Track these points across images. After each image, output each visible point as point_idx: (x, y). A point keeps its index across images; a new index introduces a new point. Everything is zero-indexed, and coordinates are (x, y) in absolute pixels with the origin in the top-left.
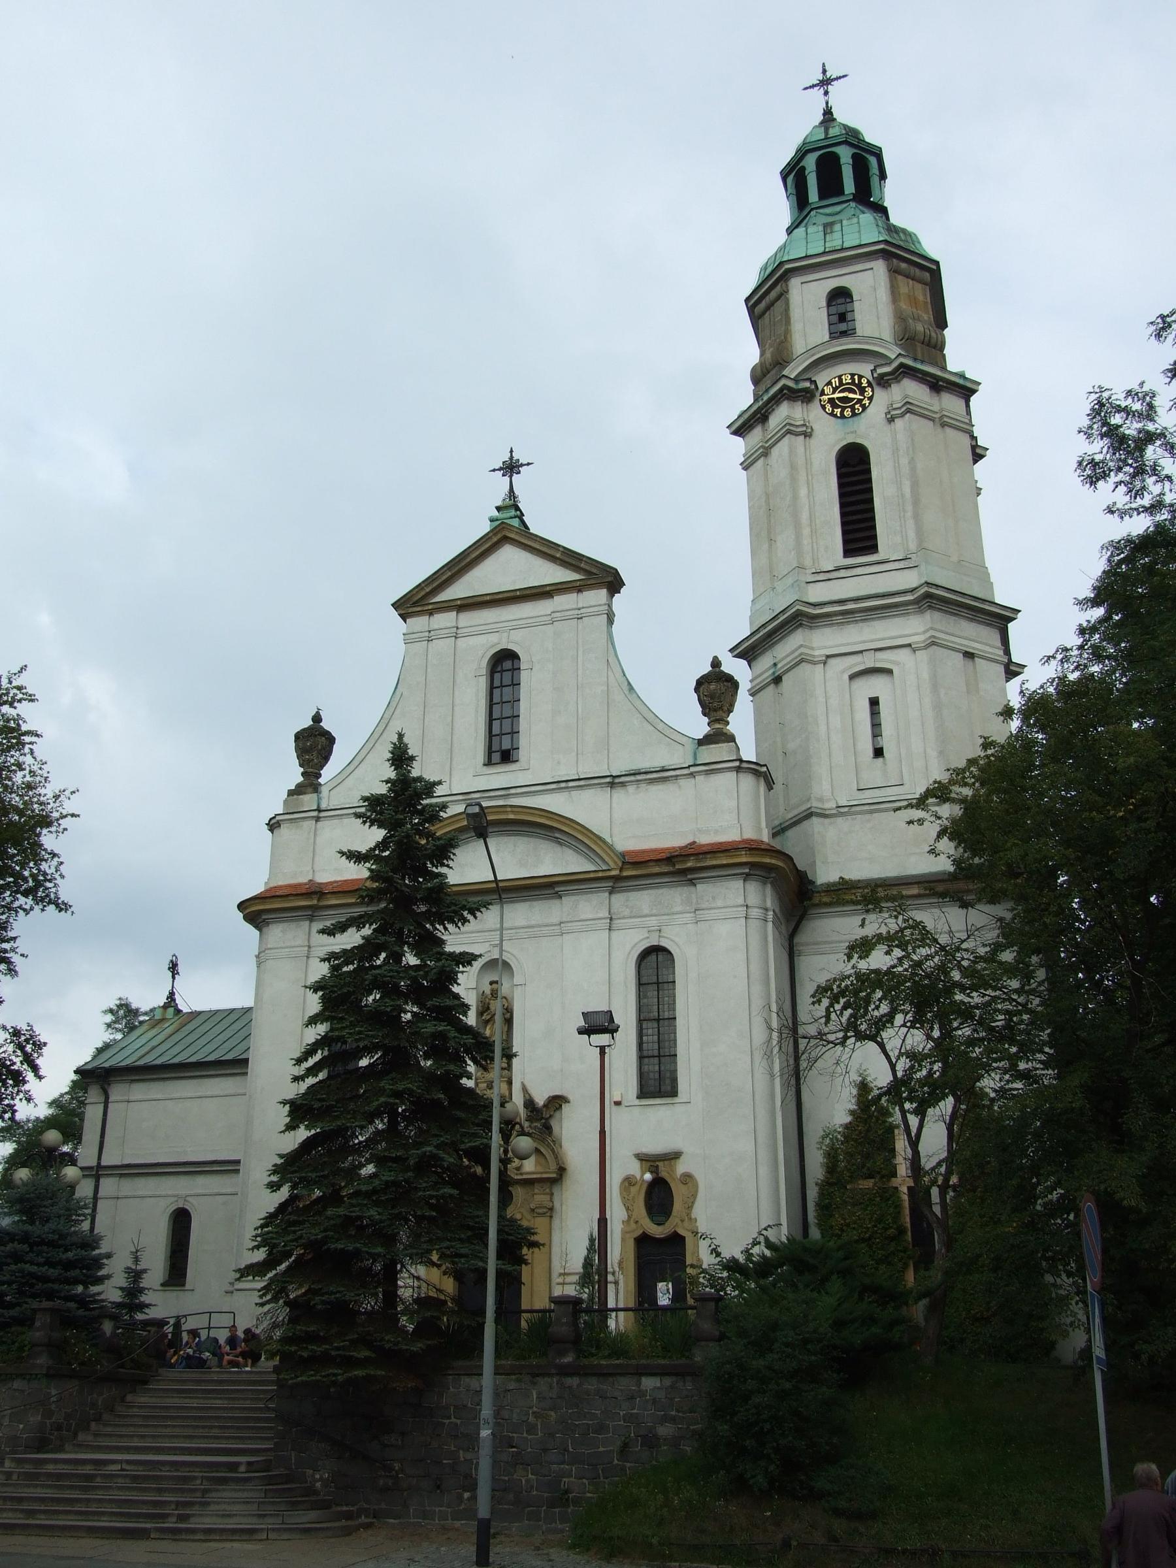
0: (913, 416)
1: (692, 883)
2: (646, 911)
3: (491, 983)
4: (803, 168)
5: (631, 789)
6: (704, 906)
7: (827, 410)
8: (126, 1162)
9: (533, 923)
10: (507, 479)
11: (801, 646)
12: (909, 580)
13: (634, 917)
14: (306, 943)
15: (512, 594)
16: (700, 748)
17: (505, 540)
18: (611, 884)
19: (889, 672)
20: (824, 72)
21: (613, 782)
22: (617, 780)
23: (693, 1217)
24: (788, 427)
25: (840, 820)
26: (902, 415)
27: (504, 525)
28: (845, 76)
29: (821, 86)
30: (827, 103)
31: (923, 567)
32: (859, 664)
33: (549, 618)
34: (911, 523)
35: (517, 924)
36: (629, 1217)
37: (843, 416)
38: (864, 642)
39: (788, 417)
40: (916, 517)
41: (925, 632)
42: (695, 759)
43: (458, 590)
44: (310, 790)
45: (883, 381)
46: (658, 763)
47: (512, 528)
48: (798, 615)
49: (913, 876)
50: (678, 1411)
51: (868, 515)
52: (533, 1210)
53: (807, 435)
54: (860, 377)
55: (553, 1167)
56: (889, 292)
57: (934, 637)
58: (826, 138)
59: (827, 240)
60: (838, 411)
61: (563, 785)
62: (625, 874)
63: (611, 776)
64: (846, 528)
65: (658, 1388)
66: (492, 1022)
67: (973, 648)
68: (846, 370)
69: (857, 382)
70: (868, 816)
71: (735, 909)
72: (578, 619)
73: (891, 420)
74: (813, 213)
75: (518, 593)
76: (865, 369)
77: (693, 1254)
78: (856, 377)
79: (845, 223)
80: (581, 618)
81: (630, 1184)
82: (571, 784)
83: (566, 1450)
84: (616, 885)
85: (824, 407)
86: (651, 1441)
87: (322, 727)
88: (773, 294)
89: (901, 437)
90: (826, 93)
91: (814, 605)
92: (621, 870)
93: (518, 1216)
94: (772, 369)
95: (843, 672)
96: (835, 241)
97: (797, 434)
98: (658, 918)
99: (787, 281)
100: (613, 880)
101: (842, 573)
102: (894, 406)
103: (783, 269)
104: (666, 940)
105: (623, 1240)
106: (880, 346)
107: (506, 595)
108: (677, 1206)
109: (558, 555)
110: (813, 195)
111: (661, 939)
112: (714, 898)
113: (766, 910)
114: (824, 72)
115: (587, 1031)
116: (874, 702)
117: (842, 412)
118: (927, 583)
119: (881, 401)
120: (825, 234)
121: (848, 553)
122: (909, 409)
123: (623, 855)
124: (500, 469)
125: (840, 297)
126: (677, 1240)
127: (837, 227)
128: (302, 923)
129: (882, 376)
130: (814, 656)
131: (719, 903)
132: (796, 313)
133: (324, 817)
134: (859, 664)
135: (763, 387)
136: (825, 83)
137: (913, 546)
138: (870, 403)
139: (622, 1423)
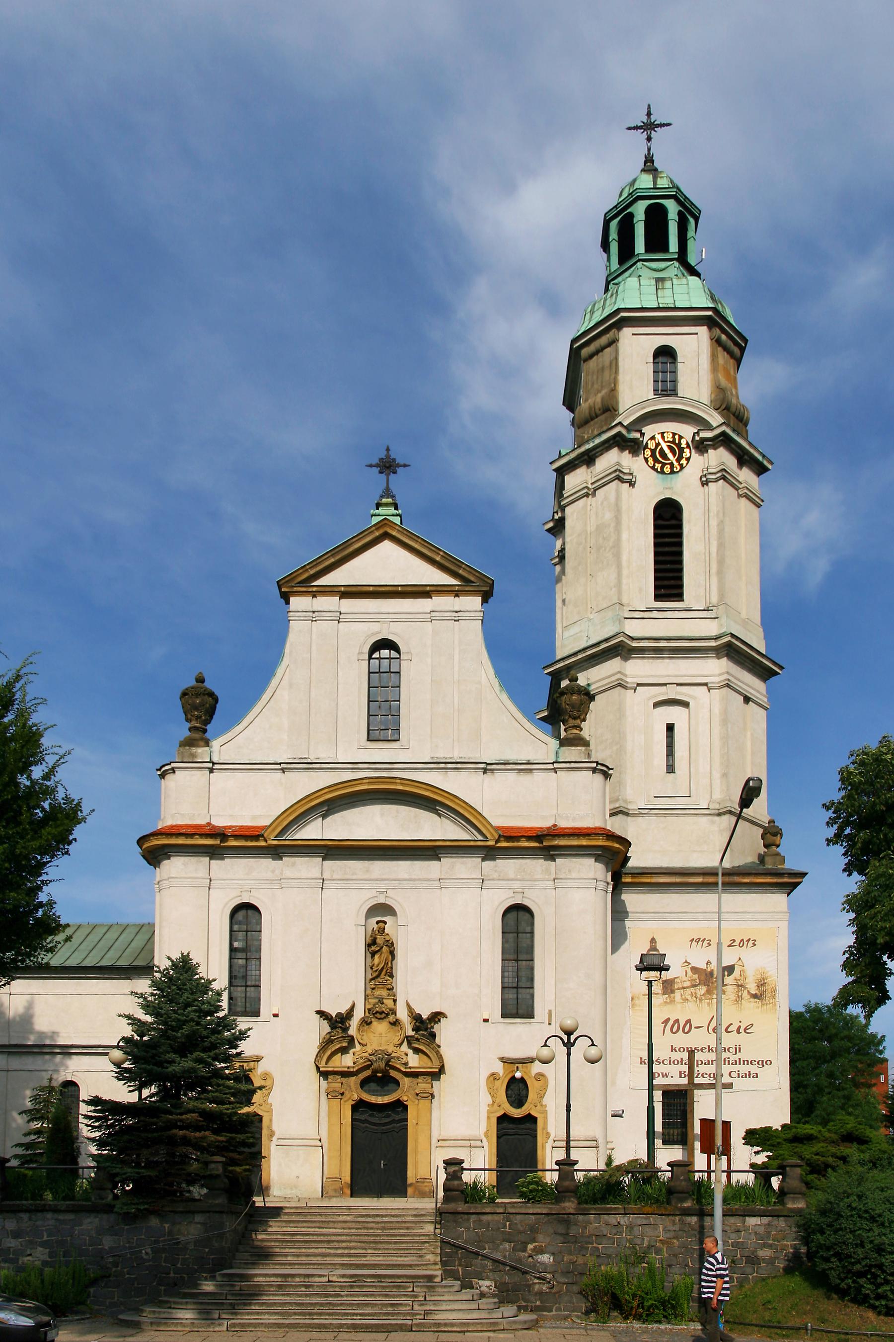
0: (725, 483)
1: (552, 858)
2: (512, 876)
3: (378, 922)
4: (631, 216)
5: (498, 775)
6: (561, 877)
7: (649, 463)
8: (12, 1043)
9: (414, 877)
10: (383, 476)
11: (619, 672)
12: (710, 628)
13: (503, 880)
14: (207, 876)
15: (421, 589)
16: (563, 749)
17: (386, 536)
18: (325, 852)
19: (686, 704)
20: (649, 114)
21: (487, 769)
22: (489, 767)
23: (544, 1104)
24: (618, 473)
25: (640, 819)
26: (717, 480)
27: (386, 522)
28: (669, 125)
29: (645, 130)
30: (649, 150)
31: (724, 619)
32: (663, 694)
33: (429, 616)
34: (714, 580)
35: (400, 877)
36: (494, 1102)
37: (662, 472)
38: (669, 676)
39: (618, 464)
40: (720, 572)
41: (720, 675)
42: (557, 757)
43: (338, 577)
44: (202, 743)
45: (701, 446)
46: (523, 757)
47: (394, 526)
48: (621, 645)
49: (696, 868)
50: (773, 1240)
51: (678, 566)
52: (417, 1095)
53: (632, 484)
54: (681, 437)
55: (437, 1064)
56: (709, 360)
57: (729, 680)
58: (655, 188)
59: (659, 296)
60: (658, 466)
61: (442, 766)
62: (499, 845)
63: (485, 763)
64: (659, 575)
65: (759, 1225)
66: (379, 953)
67: (751, 694)
68: (671, 427)
69: (677, 442)
70: (662, 818)
71: (587, 881)
72: (455, 621)
73: (705, 483)
74: (639, 264)
75: (400, 589)
76: (687, 431)
77: (543, 1129)
78: (677, 437)
79: (675, 281)
80: (458, 621)
81: (495, 1079)
82: (449, 766)
83: (687, 1265)
84: (329, 853)
85: (646, 460)
86: (753, 1260)
87: (579, 685)
88: (604, 340)
89: (713, 500)
90: (649, 139)
91: (632, 639)
92: (497, 841)
93: (405, 1098)
94: (601, 414)
95: (649, 699)
96: (666, 300)
97: (622, 481)
98: (522, 882)
99: (619, 329)
100: (487, 849)
101: (655, 614)
102: (710, 471)
103: (619, 316)
104: (391, 900)
105: (488, 1118)
106: (704, 411)
107: (415, 589)
108: (532, 1096)
109: (438, 558)
110: (640, 246)
111: (524, 899)
112: (570, 871)
113: (608, 884)
114: (649, 114)
115: (641, 968)
116: (670, 728)
117: (662, 468)
118: (733, 635)
119: (697, 464)
120: (657, 289)
121: (658, 597)
122: (724, 476)
123: (497, 829)
124: (377, 466)
125: (665, 354)
126: (531, 1119)
127: (668, 284)
128: (202, 859)
129: (704, 440)
130: (627, 682)
131: (574, 875)
132: (624, 363)
133: (217, 769)
134: (663, 694)
135: (586, 433)
136: (649, 127)
137: (714, 600)
138: (687, 464)
139: (731, 1247)
